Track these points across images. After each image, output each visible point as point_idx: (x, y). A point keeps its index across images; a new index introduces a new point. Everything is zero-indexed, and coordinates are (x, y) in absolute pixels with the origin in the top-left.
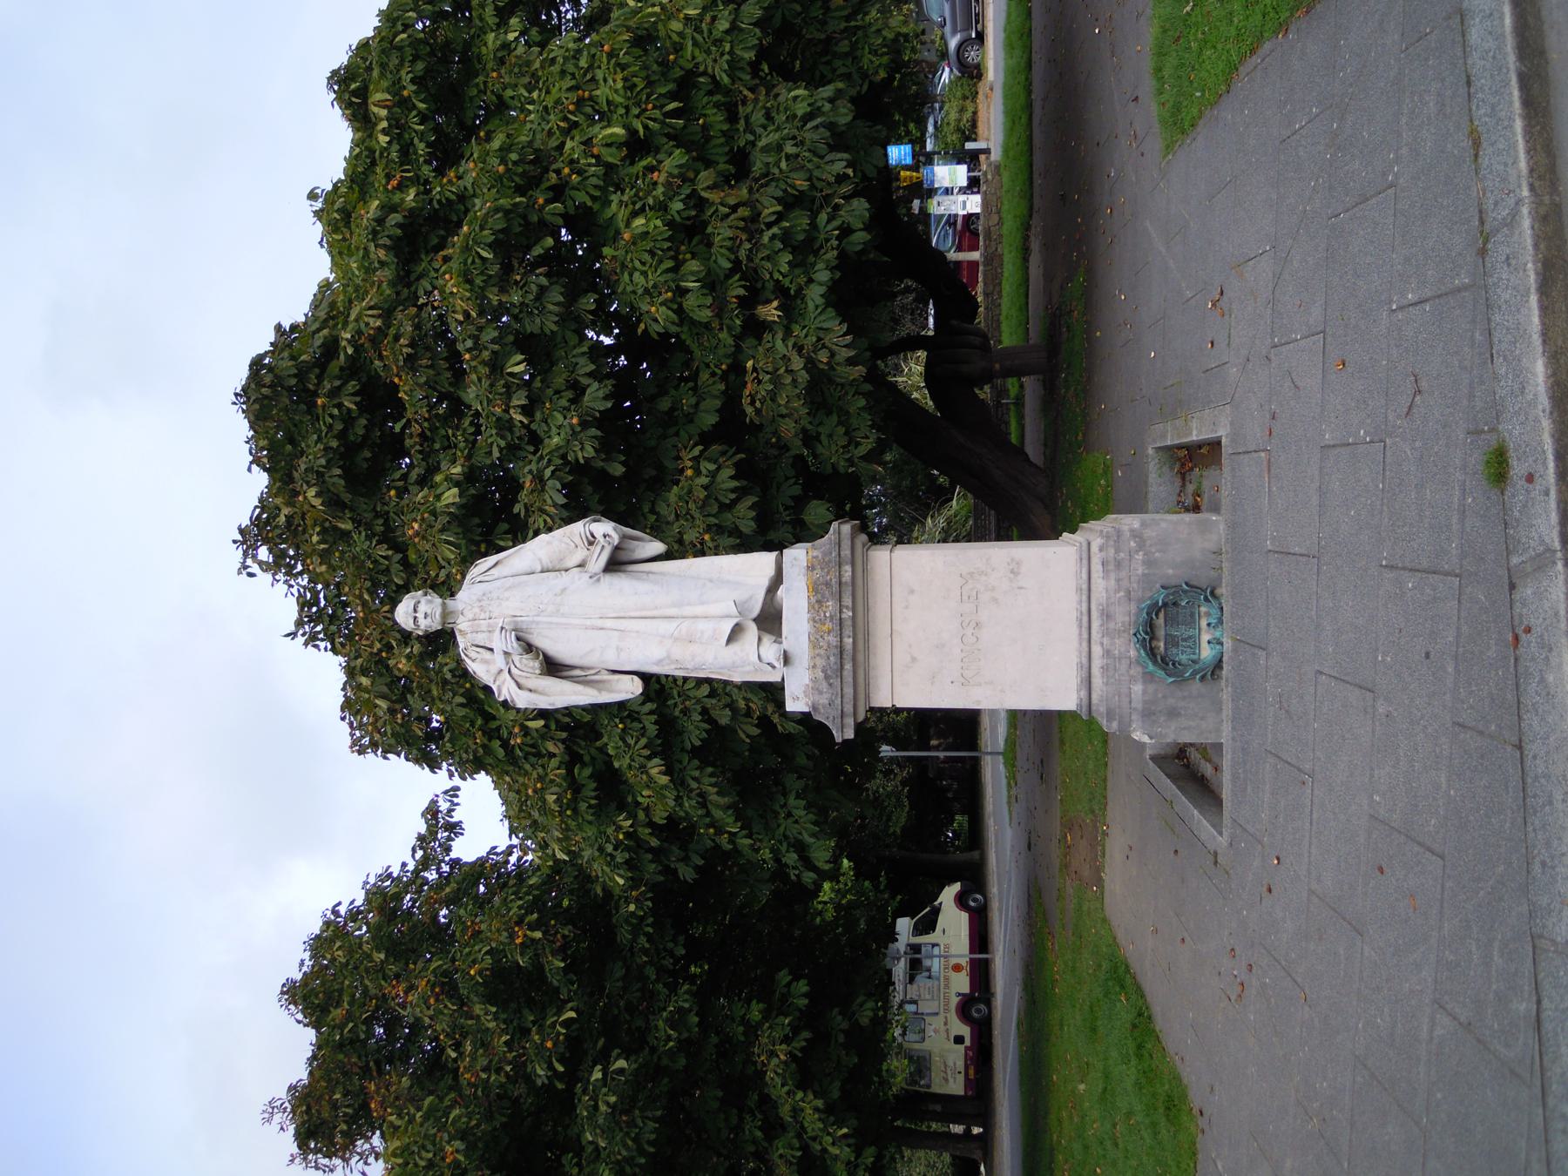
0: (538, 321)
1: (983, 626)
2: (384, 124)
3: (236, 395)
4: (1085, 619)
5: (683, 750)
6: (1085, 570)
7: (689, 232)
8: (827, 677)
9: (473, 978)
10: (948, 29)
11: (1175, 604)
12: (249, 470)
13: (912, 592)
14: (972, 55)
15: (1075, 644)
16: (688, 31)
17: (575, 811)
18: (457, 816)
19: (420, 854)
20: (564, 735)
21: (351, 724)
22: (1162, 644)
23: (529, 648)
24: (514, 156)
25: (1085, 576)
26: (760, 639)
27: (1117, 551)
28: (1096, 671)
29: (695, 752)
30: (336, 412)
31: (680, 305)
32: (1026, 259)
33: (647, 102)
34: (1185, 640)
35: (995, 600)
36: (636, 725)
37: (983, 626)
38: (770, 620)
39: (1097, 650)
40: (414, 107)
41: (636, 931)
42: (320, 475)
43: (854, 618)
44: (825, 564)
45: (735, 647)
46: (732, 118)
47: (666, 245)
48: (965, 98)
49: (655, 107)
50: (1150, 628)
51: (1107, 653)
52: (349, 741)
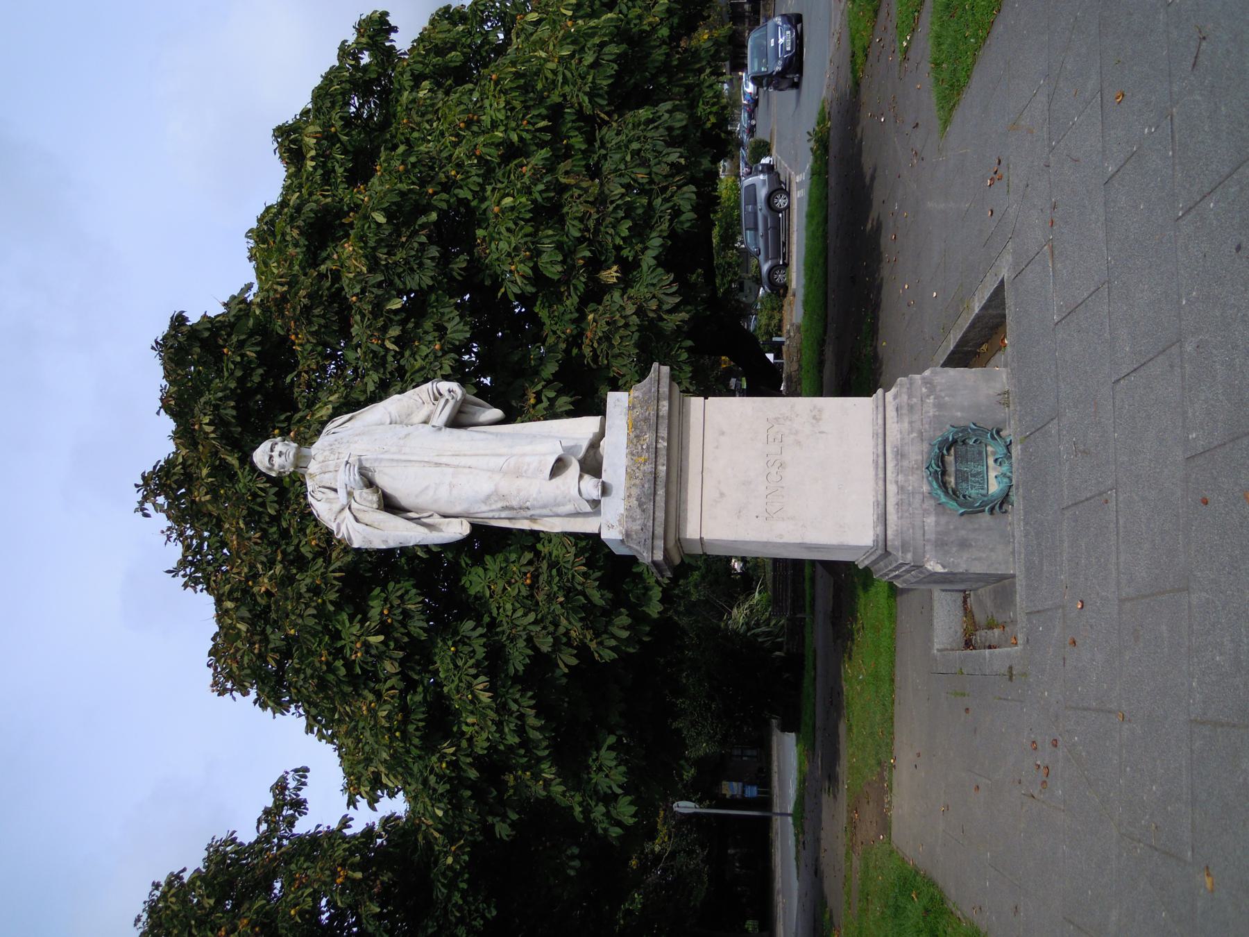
0: (417, 277)
1: (788, 475)
2: (313, 153)
3: (157, 343)
4: (881, 460)
5: (507, 675)
6: (880, 416)
7: (548, 213)
8: (640, 505)
9: (292, 918)
10: (762, 257)
11: (964, 442)
12: (158, 413)
13: (723, 433)
14: (780, 277)
15: (872, 483)
16: (561, 69)
17: (404, 732)
18: (303, 794)
19: (264, 827)
20: (401, 654)
21: (215, 669)
22: (952, 480)
23: (370, 484)
24: (413, 159)
25: (880, 422)
26: (581, 477)
27: (910, 396)
28: (891, 508)
29: (516, 679)
30: (238, 359)
31: (536, 264)
32: (821, 371)
33: (523, 119)
34: (974, 476)
35: (799, 443)
36: (466, 649)
37: (788, 475)
38: (592, 465)
39: (892, 489)
40: (339, 140)
41: (452, 886)
42: (216, 407)
43: (669, 448)
44: (645, 403)
45: (558, 481)
46: (590, 140)
47: (528, 216)
48: (773, 309)
49: (529, 123)
50: (941, 460)
51: (901, 489)
52: (211, 681)
